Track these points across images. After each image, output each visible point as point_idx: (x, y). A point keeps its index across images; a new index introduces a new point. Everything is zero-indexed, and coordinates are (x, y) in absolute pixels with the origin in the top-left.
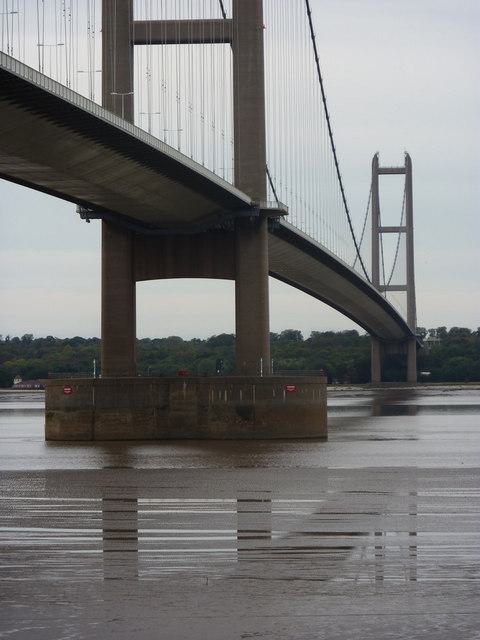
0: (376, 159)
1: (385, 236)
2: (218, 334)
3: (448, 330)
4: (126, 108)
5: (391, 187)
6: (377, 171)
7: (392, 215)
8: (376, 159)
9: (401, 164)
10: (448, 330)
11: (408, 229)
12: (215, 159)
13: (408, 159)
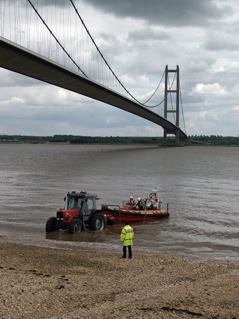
0: (167, 67)
4: (178, 126)
8: (167, 67)
12: (175, 124)
13: (178, 67)
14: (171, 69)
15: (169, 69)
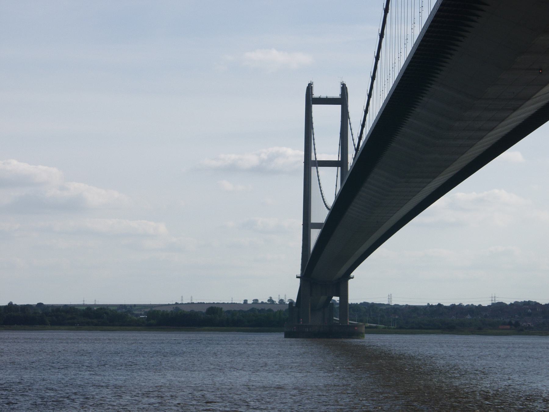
0: (310, 88)
8: (310, 88)
9: (337, 94)
13: (344, 88)
14: (324, 95)
15: (316, 94)
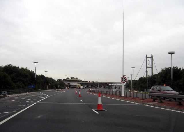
0: (147, 56)
1: (148, 69)
2: (25, 68)
3: (181, 69)
5: (149, 60)
6: (147, 57)
7: (149, 65)
8: (147, 56)
9: (151, 56)
10: (181, 69)
11: (152, 67)
13: (152, 55)
